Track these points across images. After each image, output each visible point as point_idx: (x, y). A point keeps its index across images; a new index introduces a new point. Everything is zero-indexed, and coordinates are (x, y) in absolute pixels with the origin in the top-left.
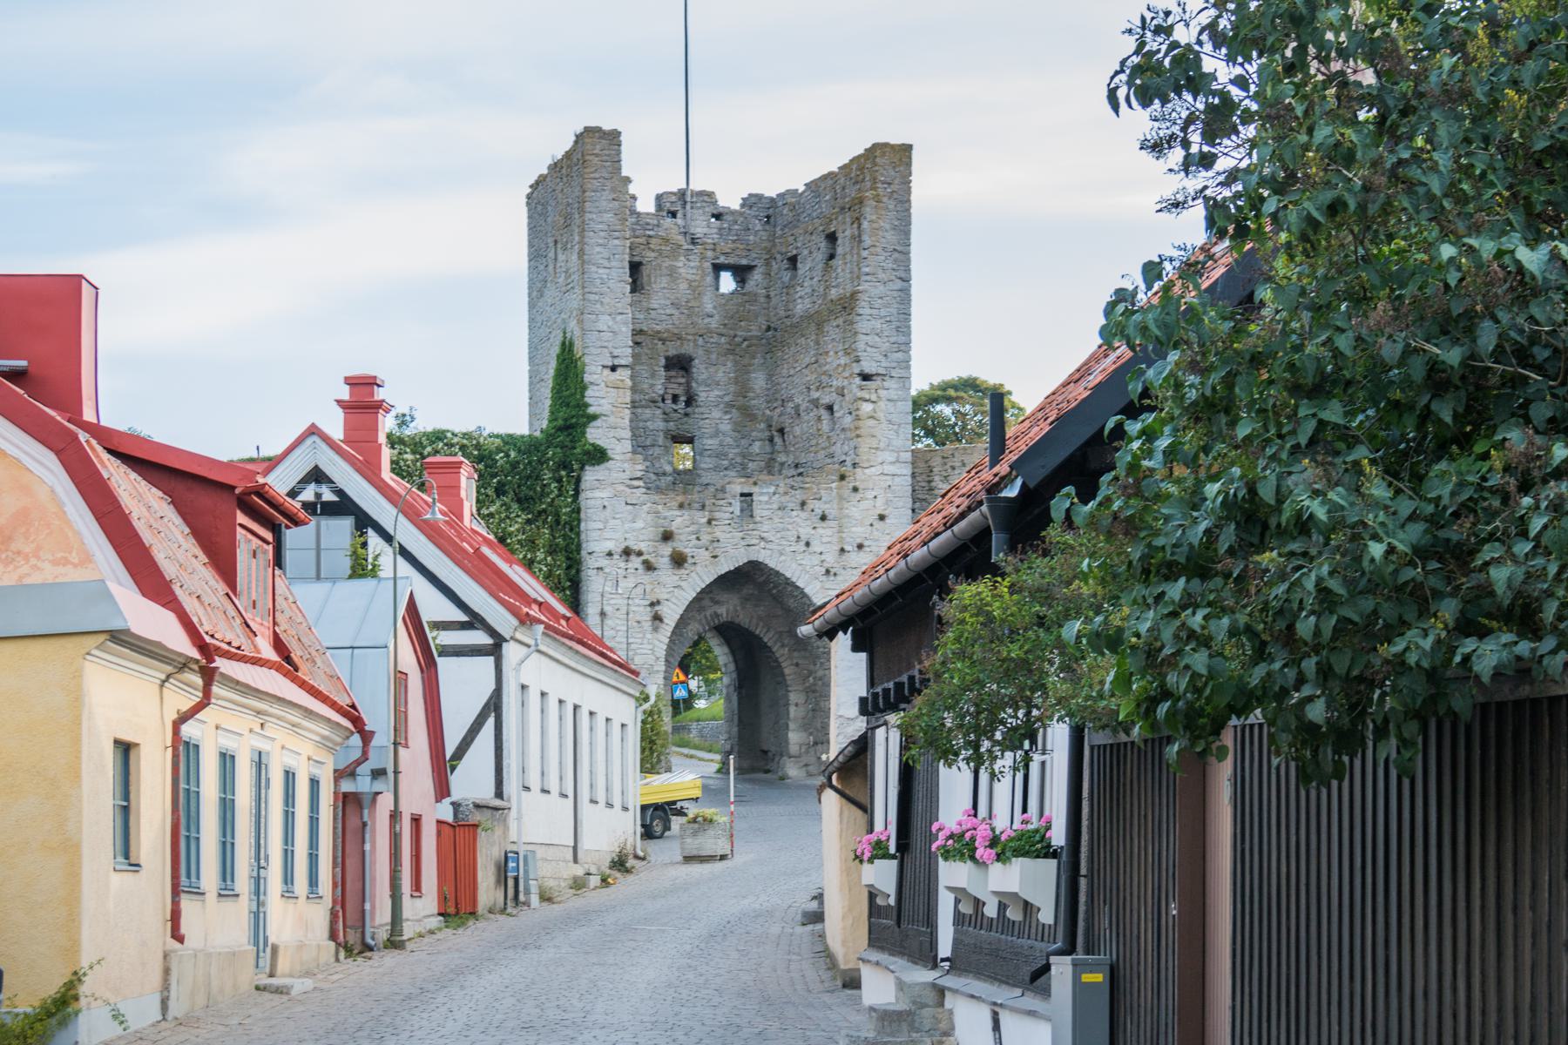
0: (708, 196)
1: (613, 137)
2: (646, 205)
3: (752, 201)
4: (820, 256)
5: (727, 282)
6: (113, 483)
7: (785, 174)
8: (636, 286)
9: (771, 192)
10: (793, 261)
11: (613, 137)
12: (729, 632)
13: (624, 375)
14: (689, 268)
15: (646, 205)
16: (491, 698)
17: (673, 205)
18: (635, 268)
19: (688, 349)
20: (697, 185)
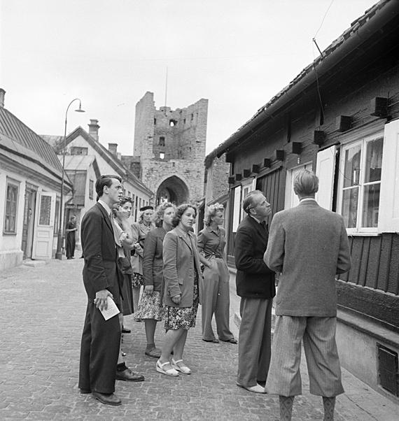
0: (169, 108)
1: (152, 94)
2: (158, 109)
3: (178, 110)
4: (190, 119)
5: (172, 124)
6: (352, 157)
7: (184, 105)
8: (155, 123)
9: (181, 108)
10: (185, 120)
11: (152, 94)
12: (167, 188)
13: (152, 139)
14: (166, 121)
15: (158, 109)
16: (88, 317)
17: (164, 109)
18: (155, 120)
19: (164, 136)
20: (167, 106)
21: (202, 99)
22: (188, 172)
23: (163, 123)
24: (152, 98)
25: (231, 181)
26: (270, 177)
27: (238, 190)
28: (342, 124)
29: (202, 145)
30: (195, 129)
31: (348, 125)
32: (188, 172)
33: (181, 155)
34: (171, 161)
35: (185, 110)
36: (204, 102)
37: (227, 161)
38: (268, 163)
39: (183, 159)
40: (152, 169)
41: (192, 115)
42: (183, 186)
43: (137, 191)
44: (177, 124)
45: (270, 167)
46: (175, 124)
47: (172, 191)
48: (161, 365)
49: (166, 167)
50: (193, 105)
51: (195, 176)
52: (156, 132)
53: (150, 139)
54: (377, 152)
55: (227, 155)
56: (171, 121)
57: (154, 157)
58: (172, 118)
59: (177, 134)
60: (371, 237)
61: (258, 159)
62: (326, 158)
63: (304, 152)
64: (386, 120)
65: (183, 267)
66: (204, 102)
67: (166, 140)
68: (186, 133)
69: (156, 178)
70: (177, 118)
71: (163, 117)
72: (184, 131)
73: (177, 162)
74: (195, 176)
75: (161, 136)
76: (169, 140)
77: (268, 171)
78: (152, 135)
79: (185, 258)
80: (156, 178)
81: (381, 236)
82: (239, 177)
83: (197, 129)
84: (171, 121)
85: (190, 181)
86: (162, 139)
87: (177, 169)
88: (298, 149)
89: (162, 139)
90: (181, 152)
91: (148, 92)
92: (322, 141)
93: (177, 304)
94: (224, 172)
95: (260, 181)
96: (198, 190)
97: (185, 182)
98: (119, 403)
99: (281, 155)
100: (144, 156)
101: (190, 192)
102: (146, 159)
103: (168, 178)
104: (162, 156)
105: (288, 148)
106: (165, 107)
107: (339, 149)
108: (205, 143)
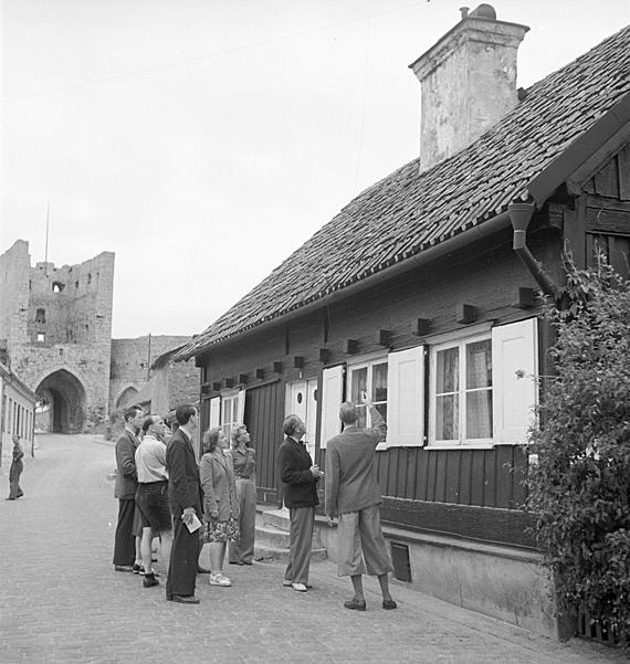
0: (52, 264)
1: (27, 243)
2: (33, 265)
3: (65, 267)
4: (86, 281)
5: (57, 289)
9: (71, 265)
10: (77, 283)
11: (27, 243)
15: (33, 265)
17: (43, 267)
21: (104, 253)
22: (84, 362)
23: (43, 287)
24: (27, 251)
25: (205, 390)
26: (263, 390)
27: (215, 402)
28: (349, 347)
29: (106, 321)
30: (93, 297)
31: (355, 348)
32: (84, 362)
33: (70, 337)
34: (57, 347)
35: (77, 268)
36: (108, 257)
37: (197, 366)
38: (261, 374)
39: (75, 342)
40: (26, 360)
41: (90, 276)
42: (76, 385)
43: (20, 397)
44: (65, 289)
45: (262, 378)
46: (61, 290)
47: (58, 392)
48: (214, 578)
49: (49, 356)
50: (90, 261)
51: (95, 369)
52: (32, 302)
53: (23, 313)
54: (381, 374)
55: (197, 358)
56: (54, 284)
57: (29, 340)
58: (56, 279)
59: (65, 304)
60: (485, 450)
61: (250, 366)
62: (333, 376)
63: (306, 367)
64: (388, 350)
65: (219, 486)
66: (108, 257)
67: (46, 313)
68: (81, 302)
69: (33, 374)
70: (64, 280)
71: (42, 278)
72: (76, 299)
73: (66, 348)
74: (95, 369)
75: (39, 307)
76: (51, 314)
77: (259, 382)
78: (26, 306)
79: (221, 477)
80: (33, 374)
81: (389, 449)
82: (217, 387)
83: (98, 298)
84: (54, 284)
85: (86, 377)
86: (41, 312)
87: (66, 358)
88: (300, 363)
89: (41, 312)
90: (70, 333)
91: (19, 241)
92: (328, 359)
93: (216, 519)
94: (183, 376)
95: (253, 393)
96: (99, 391)
97: (79, 378)
98: (198, 602)
99: (279, 368)
100: (13, 340)
101: (88, 394)
102: (17, 344)
103: (52, 374)
104: (41, 338)
105: (290, 360)
106: (46, 263)
107: (345, 369)
108: (110, 319)
